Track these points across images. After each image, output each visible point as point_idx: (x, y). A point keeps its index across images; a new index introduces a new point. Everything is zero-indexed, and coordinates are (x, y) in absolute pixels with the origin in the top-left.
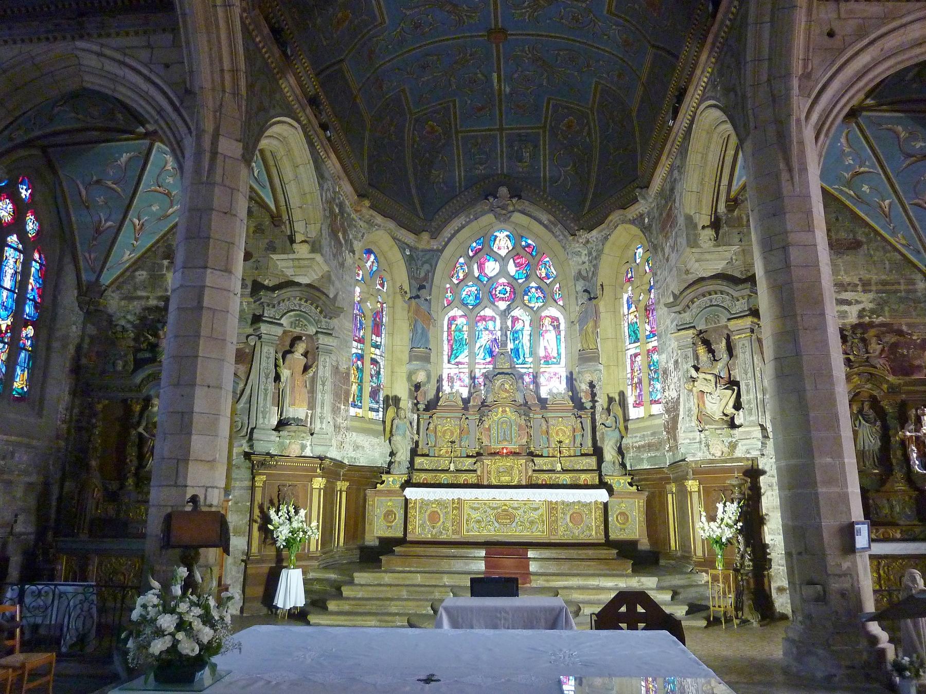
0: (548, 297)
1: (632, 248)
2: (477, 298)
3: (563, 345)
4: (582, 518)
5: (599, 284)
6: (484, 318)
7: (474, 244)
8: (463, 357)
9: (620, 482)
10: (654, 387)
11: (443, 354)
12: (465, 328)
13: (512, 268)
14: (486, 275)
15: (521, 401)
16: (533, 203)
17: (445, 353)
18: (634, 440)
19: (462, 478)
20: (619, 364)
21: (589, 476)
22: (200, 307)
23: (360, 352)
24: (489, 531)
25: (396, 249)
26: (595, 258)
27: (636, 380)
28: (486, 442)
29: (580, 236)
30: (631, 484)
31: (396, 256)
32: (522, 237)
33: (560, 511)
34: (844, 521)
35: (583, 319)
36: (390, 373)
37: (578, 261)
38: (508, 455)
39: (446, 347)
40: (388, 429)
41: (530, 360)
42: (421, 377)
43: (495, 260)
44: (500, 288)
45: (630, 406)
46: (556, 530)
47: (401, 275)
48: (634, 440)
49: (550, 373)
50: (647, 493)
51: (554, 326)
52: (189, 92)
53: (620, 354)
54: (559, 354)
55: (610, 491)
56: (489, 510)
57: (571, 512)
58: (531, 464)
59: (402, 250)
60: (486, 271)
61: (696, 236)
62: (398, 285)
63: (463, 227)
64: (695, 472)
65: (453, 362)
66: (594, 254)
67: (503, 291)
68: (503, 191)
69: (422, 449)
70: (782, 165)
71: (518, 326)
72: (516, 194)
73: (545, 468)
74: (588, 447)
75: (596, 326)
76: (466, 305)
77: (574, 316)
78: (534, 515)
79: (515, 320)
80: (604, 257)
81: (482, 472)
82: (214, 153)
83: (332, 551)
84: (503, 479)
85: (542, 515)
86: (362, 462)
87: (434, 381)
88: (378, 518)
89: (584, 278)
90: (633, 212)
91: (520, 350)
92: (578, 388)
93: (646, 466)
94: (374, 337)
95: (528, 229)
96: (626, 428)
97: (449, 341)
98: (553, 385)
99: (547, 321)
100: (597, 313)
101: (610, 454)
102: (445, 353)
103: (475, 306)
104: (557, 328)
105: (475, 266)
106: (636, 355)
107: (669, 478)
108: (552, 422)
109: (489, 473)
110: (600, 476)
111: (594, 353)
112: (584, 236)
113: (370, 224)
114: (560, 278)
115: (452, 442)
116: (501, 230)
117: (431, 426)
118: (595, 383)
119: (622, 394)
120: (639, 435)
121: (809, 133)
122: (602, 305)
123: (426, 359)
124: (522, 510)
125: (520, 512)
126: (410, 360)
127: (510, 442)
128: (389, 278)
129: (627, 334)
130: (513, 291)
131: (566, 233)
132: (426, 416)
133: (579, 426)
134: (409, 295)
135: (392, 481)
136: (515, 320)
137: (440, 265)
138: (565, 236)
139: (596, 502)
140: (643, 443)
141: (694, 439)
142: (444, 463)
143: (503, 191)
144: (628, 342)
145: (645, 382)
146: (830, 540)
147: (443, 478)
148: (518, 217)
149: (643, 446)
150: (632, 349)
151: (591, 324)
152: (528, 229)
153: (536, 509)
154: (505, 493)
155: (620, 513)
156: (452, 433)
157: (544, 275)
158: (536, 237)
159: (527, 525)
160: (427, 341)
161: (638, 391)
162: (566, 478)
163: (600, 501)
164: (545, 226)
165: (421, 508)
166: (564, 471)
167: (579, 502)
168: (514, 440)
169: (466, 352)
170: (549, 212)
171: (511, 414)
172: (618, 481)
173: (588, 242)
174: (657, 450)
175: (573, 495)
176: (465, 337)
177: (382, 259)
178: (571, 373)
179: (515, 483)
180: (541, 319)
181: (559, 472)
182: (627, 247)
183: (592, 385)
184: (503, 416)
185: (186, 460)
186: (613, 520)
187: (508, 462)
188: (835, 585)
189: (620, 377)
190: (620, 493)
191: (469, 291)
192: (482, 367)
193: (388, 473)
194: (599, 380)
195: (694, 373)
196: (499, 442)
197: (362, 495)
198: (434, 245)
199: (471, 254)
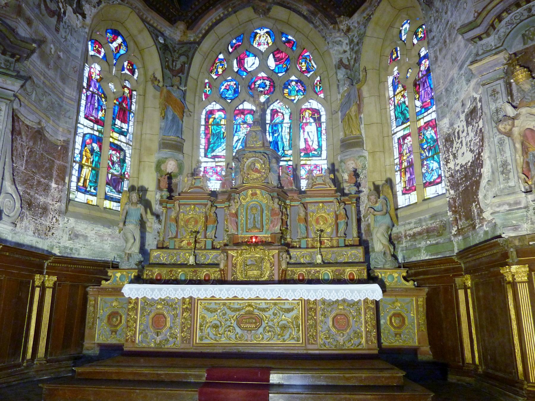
0: (307, 88)
1: (396, 26)
2: (236, 92)
3: (324, 137)
4: (348, 321)
5: (362, 68)
6: (243, 112)
7: (234, 41)
9: (395, 277)
10: (428, 167)
11: (199, 148)
12: (223, 122)
13: (271, 63)
14: (245, 70)
17: (202, 147)
18: (408, 227)
19: (203, 273)
20: (386, 150)
21: (355, 269)
23: (97, 133)
24: (229, 338)
25: (146, 34)
26: (356, 47)
27: (405, 164)
29: (341, 22)
32: (282, 33)
33: (319, 312)
35: (345, 105)
36: (137, 162)
37: (339, 49)
38: (256, 244)
39: (203, 141)
41: (290, 152)
42: (171, 166)
43: (255, 56)
44: (259, 82)
45: (399, 194)
46: (315, 337)
48: (408, 227)
49: (310, 165)
50: (426, 290)
51: (314, 119)
53: (386, 139)
54: (320, 146)
56: (228, 312)
57: (334, 314)
58: (285, 255)
59: (155, 38)
60: (246, 66)
62: (150, 73)
63: (221, 20)
64: (520, 253)
65: (210, 156)
66: (356, 40)
67: (263, 85)
71: (277, 119)
73: (302, 261)
75: (359, 110)
77: (336, 105)
78: (287, 318)
79: (274, 112)
80: (366, 40)
81: (226, 266)
83: (19, 365)
84: (250, 273)
85: (297, 318)
86: (84, 253)
88: (101, 320)
89: (346, 67)
91: (280, 143)
92: (340, 179)
93: (424, 256)
94: (118, 122)
95: (287, 23)
97: (206, 134)
99: (307, 114)
100: (360, 97)
101: (379, 244)
102: (202, 147)
104: (318, 121)
105: (235, 62)
106: (404, 137)
107: (460, 269)
108: (311, 208)
109: (234, 266)
110: (369, 269)
111: (358, 138)
112: (344, 23)
115: (195, 232)
116: (261, 28)
118: (359, 171)
119: (390, 182)
120: (413, 220)
123: (178, 147)
124: (271, 312)
127: (261, 230)
128: (140, 66)
129: (393, 118)
130: (273, 85)
133: (343, 212)
136: (274, 112)
137: (197, 59)
138: (325, 25)
139: (366, 301)
140: (419, 229)
141: (517, 203)
144: (394, 124)
145: (417, 164)
147: (181, 273)
148: (279, 12)
149: (420, 233)
151: (354, 108)
152: (287, 23)
153: (289, 310)
154: (153, 290)
155: (394, 315)
156: (196, 222)
157: (304, 69)
158: (297, 30)
159: (278, 330)
161: (408, 175)
163: (371, 298)
164: (305, 17)
165: (143, 309)
166: (325, 264)
167: (344, 301)
168: (265, 228)
169: (224, 146)
171: (262, 198)
172: (391, 275)
173: (349, 30)
174: (440, 235)
175: (316, 291)
176: (223, 130)
177: (131, 44)
178: (333, 165)
179: (266, 278)
180: (302, 111)
181: (318, 265)
186: (385, 323)
187: (258, 253)
189: (387, 163)
190: (393, 290)
194: (364, 168)
197: (80, 292)
198: (191, 37)
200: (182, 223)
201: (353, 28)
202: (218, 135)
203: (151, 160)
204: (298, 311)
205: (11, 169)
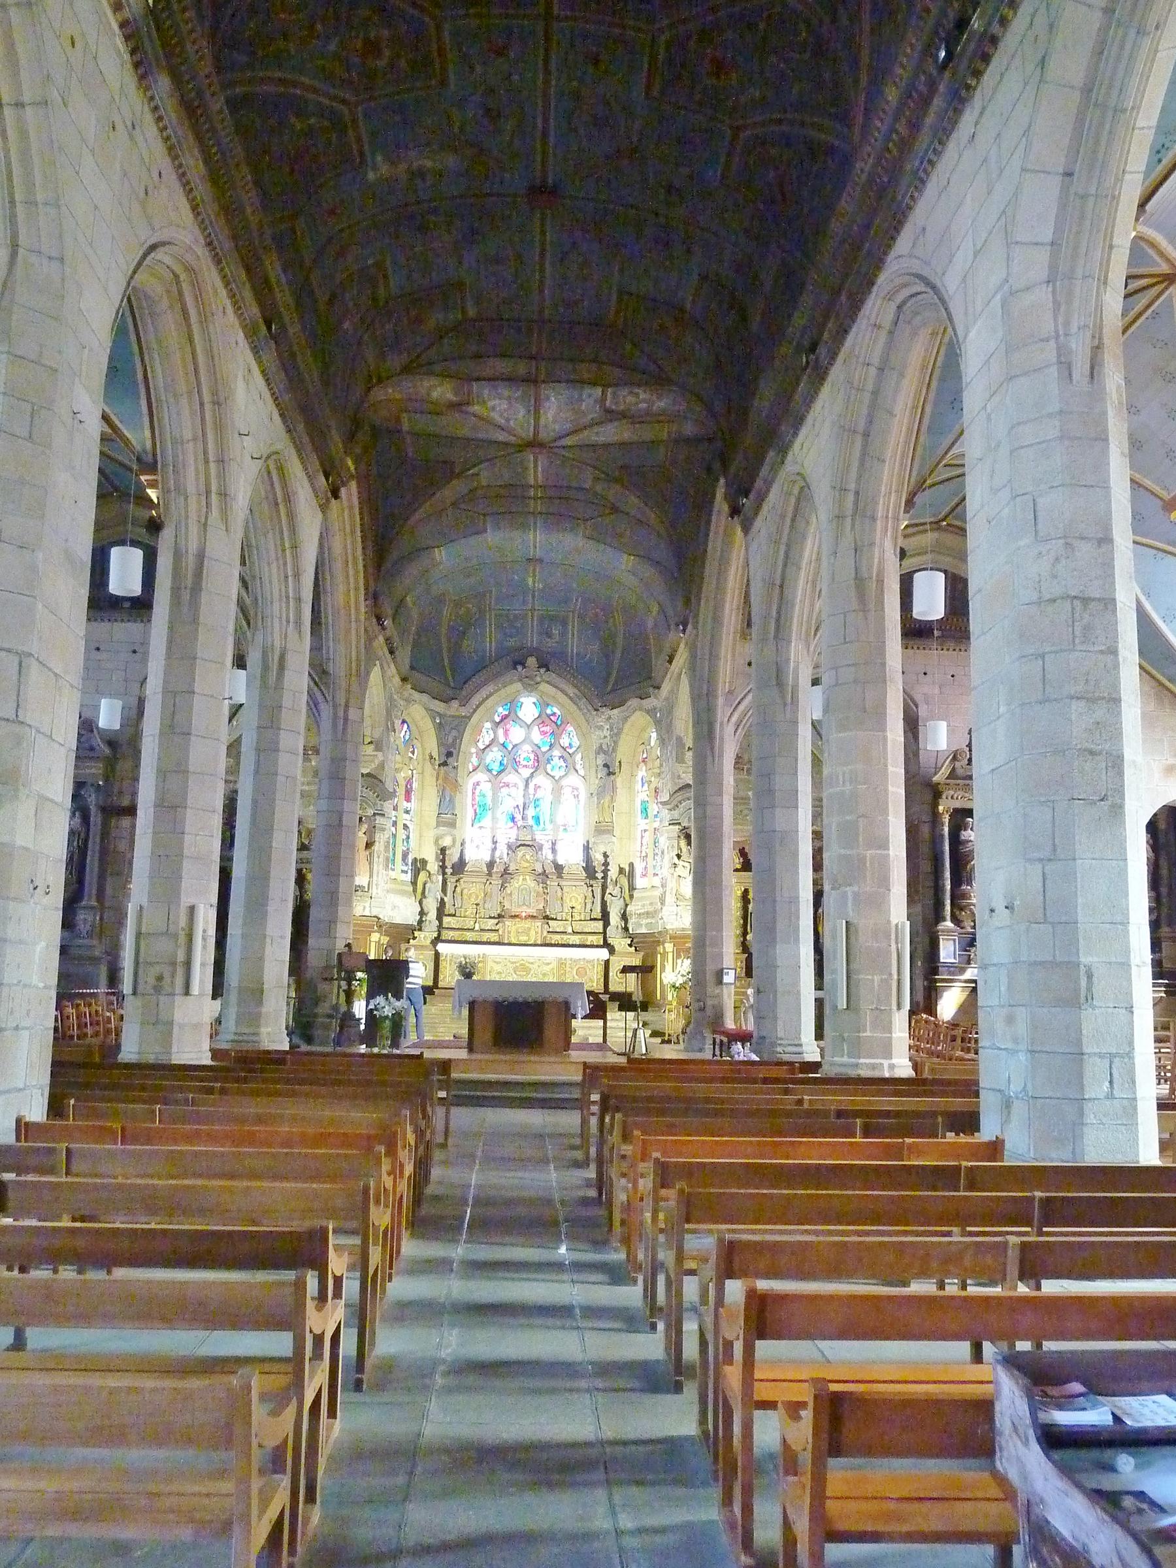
0: (571, 767)
8: (487, 821)
9: (620, 943)
13: (536, 735)
15: (540, 871)
16: (560, 675)
19: (485, 937)
22: (340, 825)
26: (616, 734)
28: (507, 906)
30: (630, 945)
31: (427, 726)
34: (719, 967)
37: (600, 736)
40: (419, 890)
42: (447, 842)
44: (524, 755)
47: (431, 744)
52: (325, 672)
55: (612, 950)
59: (433, 719)
61: (683, 754)
62: (427, 752)
63: (491, 695)
68: (532, 661)
69: (449, 908)
70: (709, 753)
71: (539, 794)
72: (544, 665)
74: (597, 913)
75: (612, 800)
76: (490, 771)
77: (594, 789)
79: (537, 787)
80: (623, 736)
82: (346, 719)
86: (398, 920)
87: (458, 844)
89: (605, 753)
90: (648, 703)
93: (644, 931)
96: (631, 897)
98: (571, 856)
100: (614, 789)
101: (615, 919)
103: (500, 773)
109: (509, 932)
113: (408, 701)
114: (582, 749)
117: (458, 890)
119: (631, 865)
121: (730, 729)
122: (619, 780)
123: (452, 825)
125: (535, 966)
126: (438, 826)
131: (590, 708)
132: (453, 879)
134: (437, 763)
135: (425, 936)
136: (537, 787)
142: (469, 924)
143: (532, 661)
146: (710, 978)
147: (469, 936)
148: (544, 687)
150: (642, 824)
151: (608, 798)
158: (561, 706)
160: (453, 808)
162: (576, 939)
164: (571, 698)
170: (576, 687)
171: (531, 883)
177: (413, 728)
182: (644, 730)
183: (605, 855)
184: (523, 884)
185: (335, 922)
187: (527, 924)
188: (709, 1002)
191: (494, 756)
192: (507, 834)
193: (420, 930)
194: (612, 851)
195: (676, 860)
196: (519, 906)
198: (463, 712)
199: (497, 719)
200: (465, 897)
201: (642, 6)
202: (484, 807)
203: (430, 835)
204: (554, 965)
205: (1160, 1502)
